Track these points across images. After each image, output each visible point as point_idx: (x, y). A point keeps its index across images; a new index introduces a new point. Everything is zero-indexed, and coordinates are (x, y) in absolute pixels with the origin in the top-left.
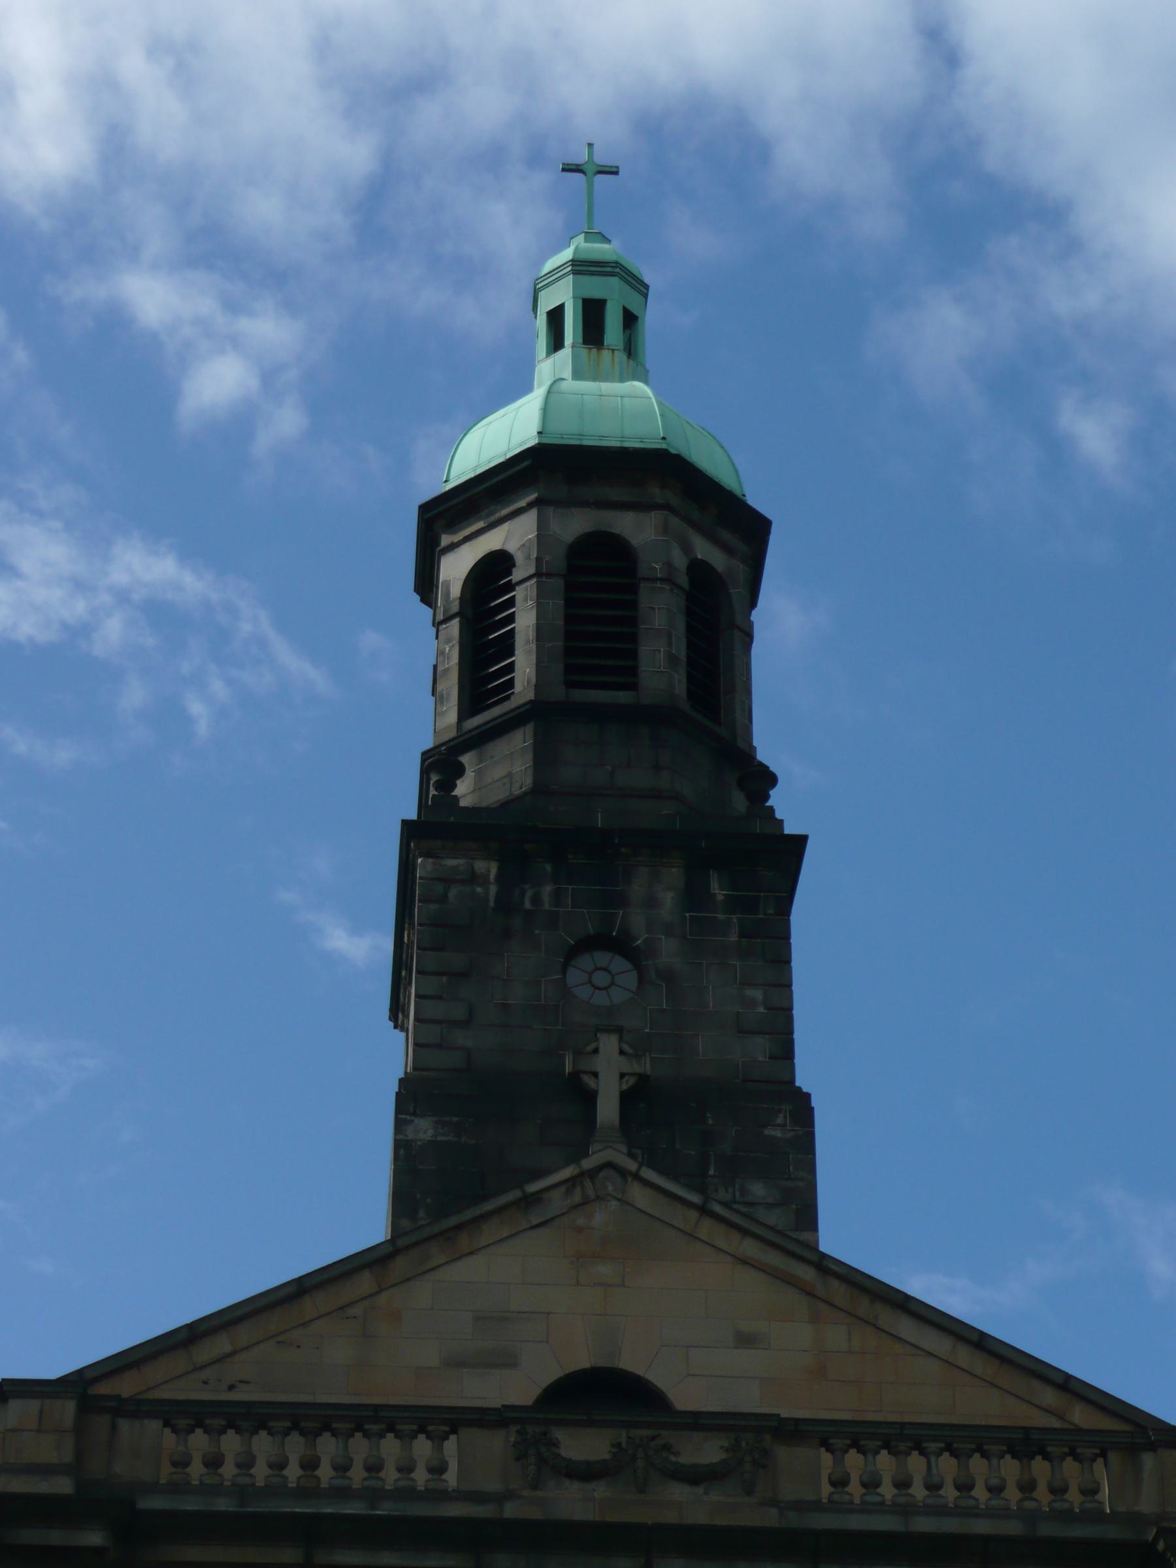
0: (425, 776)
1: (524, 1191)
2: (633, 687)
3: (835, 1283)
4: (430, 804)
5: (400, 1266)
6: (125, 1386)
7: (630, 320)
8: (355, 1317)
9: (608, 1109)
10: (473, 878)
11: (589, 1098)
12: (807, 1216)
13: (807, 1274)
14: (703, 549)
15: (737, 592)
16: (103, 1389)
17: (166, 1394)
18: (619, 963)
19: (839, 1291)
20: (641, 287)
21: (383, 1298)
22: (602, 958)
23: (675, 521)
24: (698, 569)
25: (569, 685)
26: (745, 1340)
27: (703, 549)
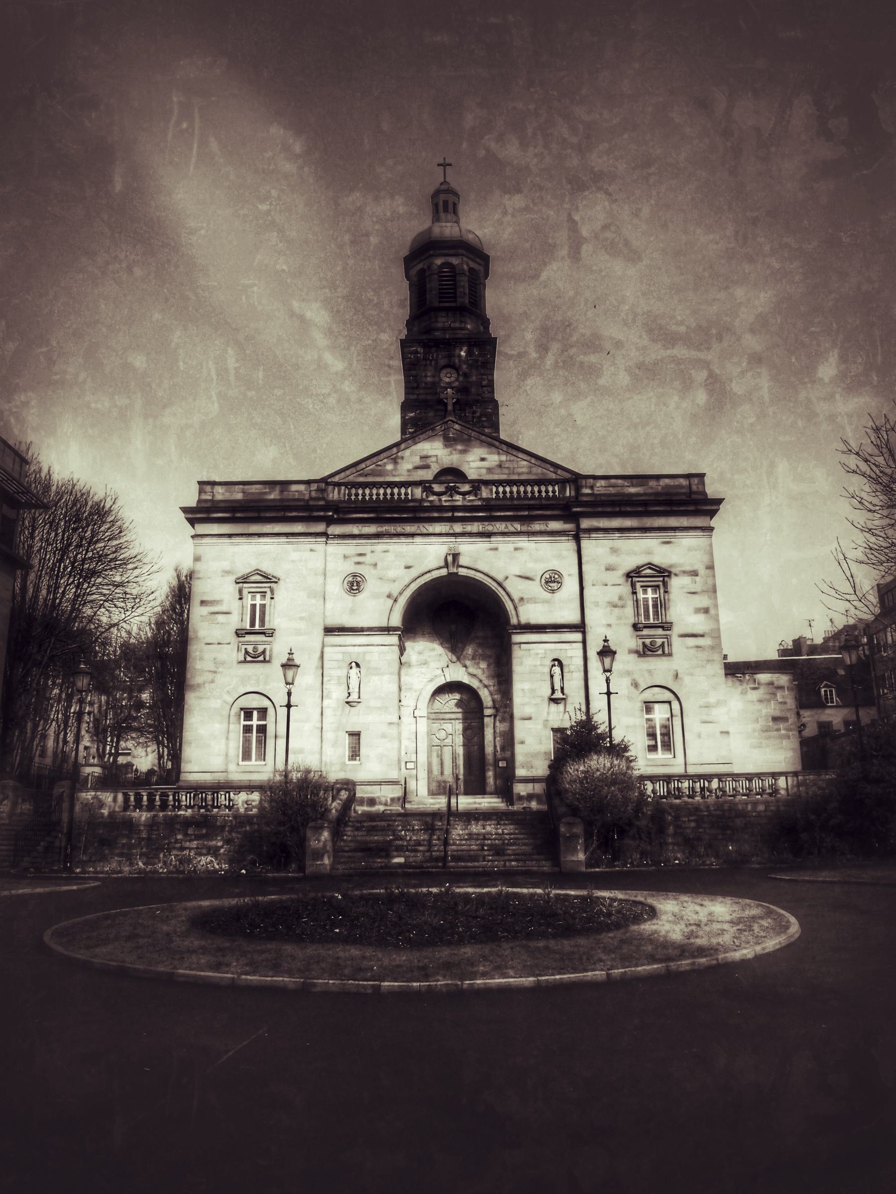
0: (316, 514)
1: (453, 514)
2: (455, 301)
3: (503, 445)
4: (574, 509)
5: (403, 446)
6: (336, 479)
7: (455, 205)
8: (381, 579)
9: (450, 408)
10: (417, 352)
11: (446, 405)
12: (497, 430)
13: (497, 443)
14: (472, 265)
15: (482, 274)
16: (329, 480)
17: (346, 480)
18: (453, 371)
19: (504, 447)
20: (456, 194)
21: (399, 454)
22: (449, 370)
23: (465, 259)
24: (471, 270)
25: (440, 302)
26: (483, 459)
27: (472, 265)
